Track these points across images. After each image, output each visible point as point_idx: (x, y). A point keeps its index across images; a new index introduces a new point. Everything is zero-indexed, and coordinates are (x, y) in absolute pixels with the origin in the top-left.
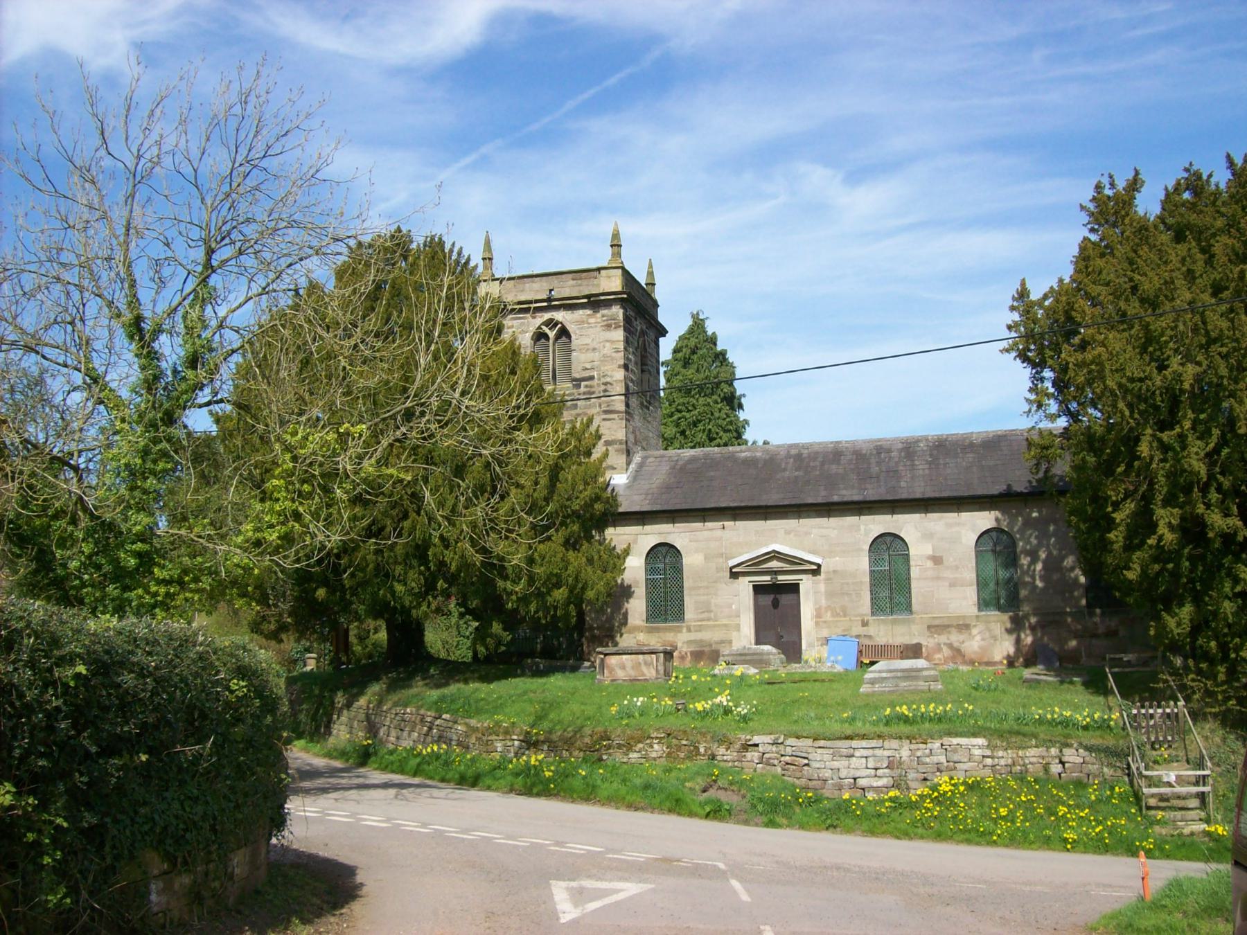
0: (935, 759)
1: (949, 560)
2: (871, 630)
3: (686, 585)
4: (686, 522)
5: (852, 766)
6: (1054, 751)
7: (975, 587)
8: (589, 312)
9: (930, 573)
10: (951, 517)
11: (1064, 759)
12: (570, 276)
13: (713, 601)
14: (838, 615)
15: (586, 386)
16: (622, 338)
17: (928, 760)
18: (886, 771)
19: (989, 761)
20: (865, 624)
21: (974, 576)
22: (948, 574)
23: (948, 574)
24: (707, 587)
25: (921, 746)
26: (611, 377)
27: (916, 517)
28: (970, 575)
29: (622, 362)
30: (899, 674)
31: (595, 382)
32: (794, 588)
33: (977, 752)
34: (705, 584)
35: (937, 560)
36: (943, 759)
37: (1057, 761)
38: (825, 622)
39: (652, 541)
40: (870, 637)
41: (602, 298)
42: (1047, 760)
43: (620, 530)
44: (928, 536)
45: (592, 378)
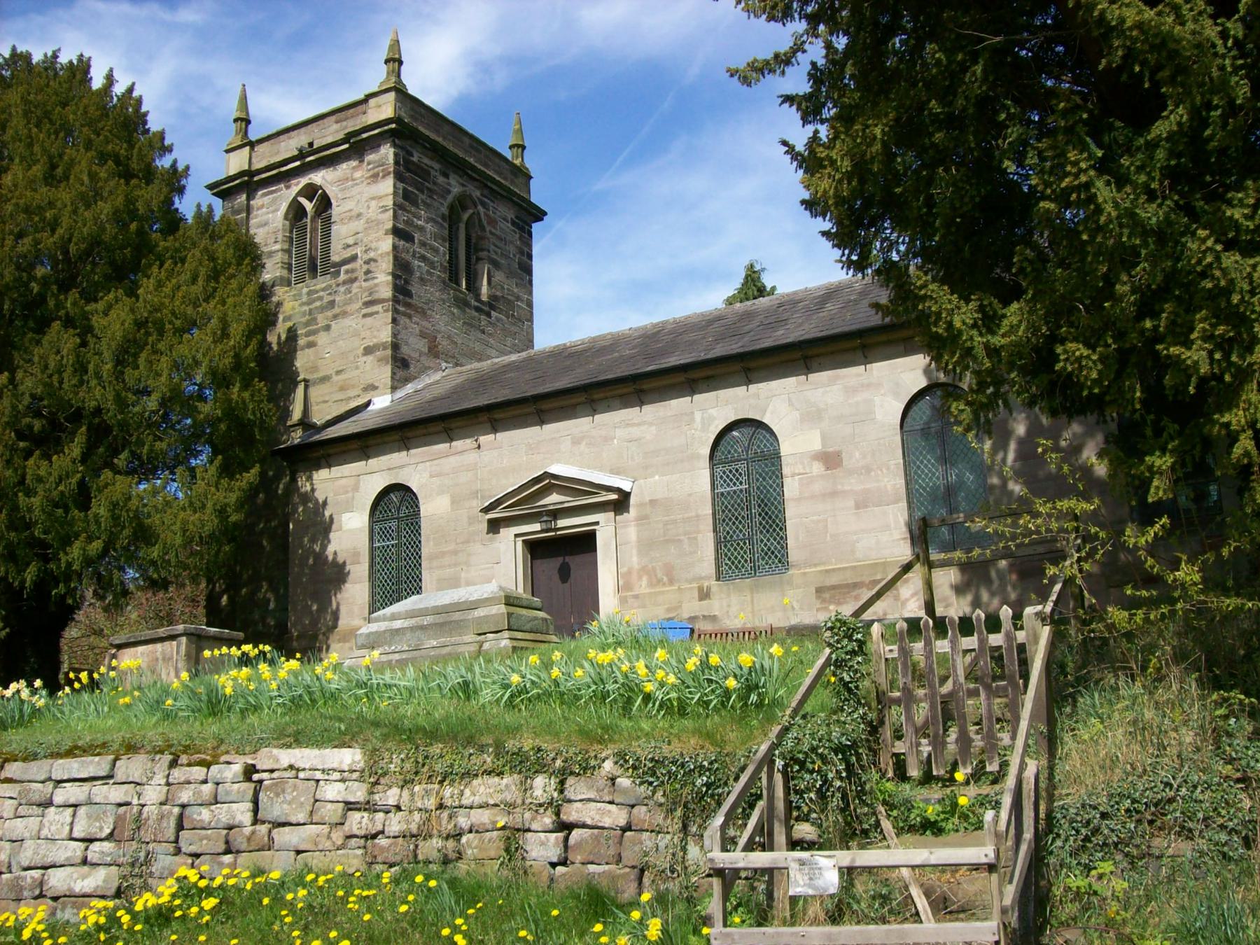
0: (223, 813)
1: (853, 458)
2: (715, 606)
3: (425, 551)
4: (425, 445)
5: (45, 832)
6: (542, 786)
7: (904, 504)
8: (354, 163)
9: (817, 487)
10: (853, 374)
11: (572, 813)
12: (333, 118)
13: (463, 575)
14: (659, 581)
15: (347, 272)
16: (391, 190)
17: (205, 815)
18: (107, 846)
19: (358, 823)
20: (704, 595)
21: (900, 482)
22: (853, 484)
23: (853, 484)
24: (455, 553)
25: (198, 772)
26: (376, 250)
27: (789, 384)
28: (895, 482)
29: (389, 225)
30: (427, 620)
31: (360, 262)
32: (585, 542)
33: (332, 791)
34: (452, 547)
35: (831, 460)
36: (241, 813)
37: (548, 820)
38: (636, 597)
39: (375, 484)
40: (713, 618)
41: (365, 136)
42: (516, 819)
43: (337, 471)
44: (812, 416)
45: (354, 258)
